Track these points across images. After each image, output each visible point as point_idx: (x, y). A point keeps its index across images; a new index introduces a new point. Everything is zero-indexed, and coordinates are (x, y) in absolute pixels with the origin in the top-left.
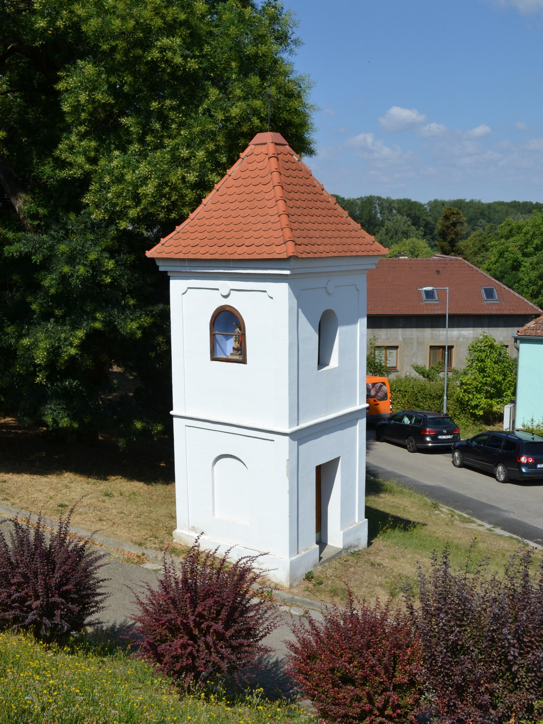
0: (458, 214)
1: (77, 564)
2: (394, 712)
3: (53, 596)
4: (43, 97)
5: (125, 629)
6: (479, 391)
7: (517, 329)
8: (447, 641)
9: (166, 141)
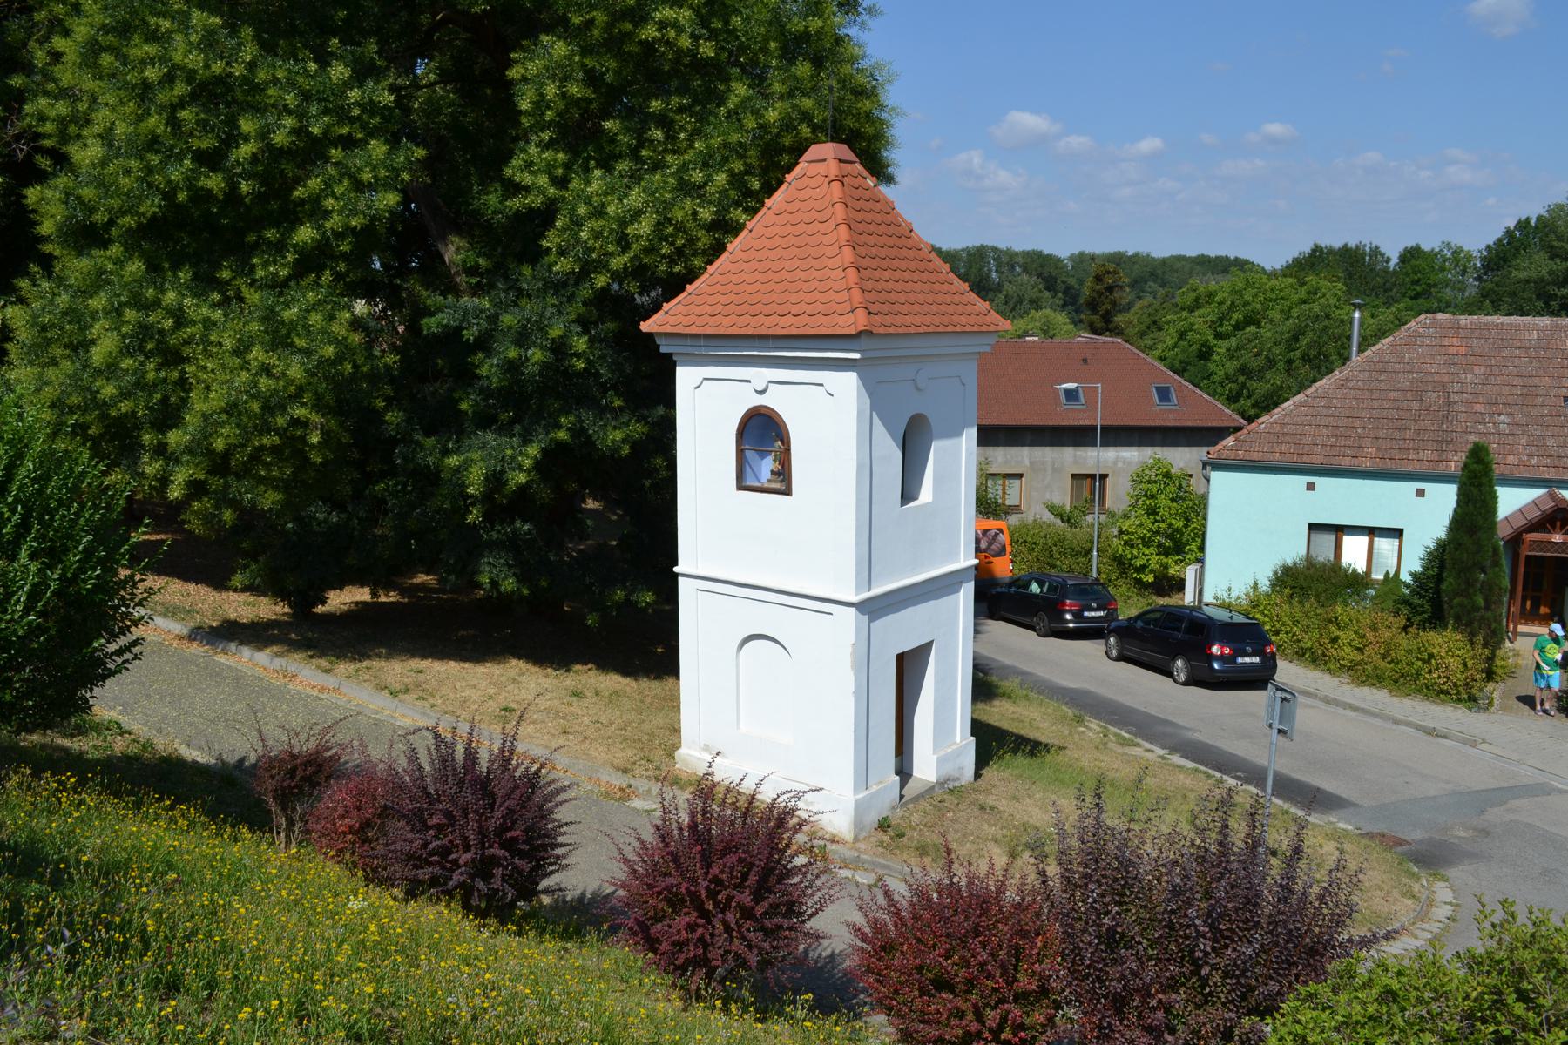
0: (1115, 272)
1: (529, 799)
2: (1015, 1035)
3: (491, 846)
4: (489, 92)
5: (599, 900)
6: (1147, 543)
7: (1205, 449)
8: (1100, 926)
9: (669, 158)
